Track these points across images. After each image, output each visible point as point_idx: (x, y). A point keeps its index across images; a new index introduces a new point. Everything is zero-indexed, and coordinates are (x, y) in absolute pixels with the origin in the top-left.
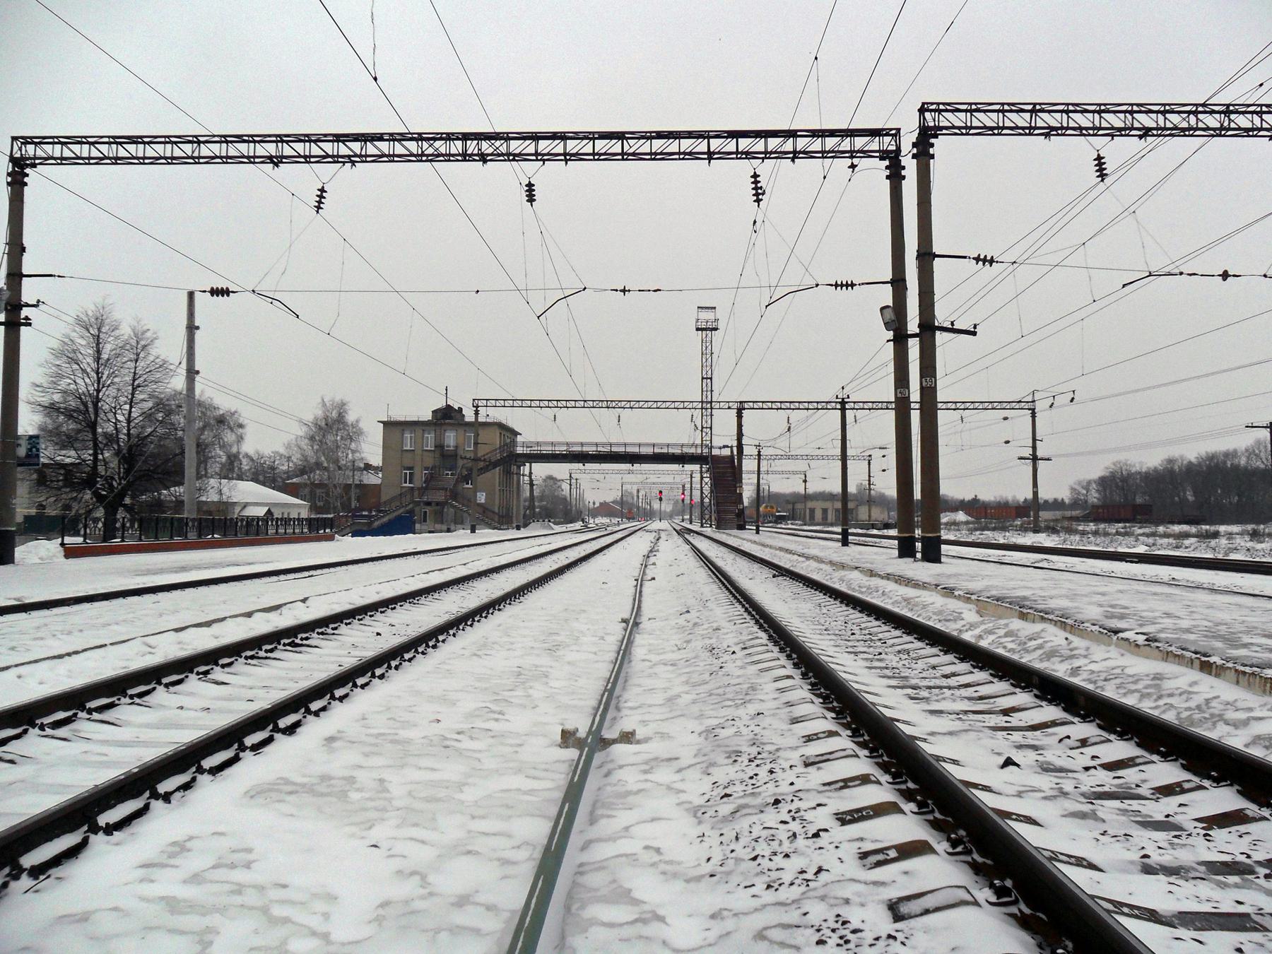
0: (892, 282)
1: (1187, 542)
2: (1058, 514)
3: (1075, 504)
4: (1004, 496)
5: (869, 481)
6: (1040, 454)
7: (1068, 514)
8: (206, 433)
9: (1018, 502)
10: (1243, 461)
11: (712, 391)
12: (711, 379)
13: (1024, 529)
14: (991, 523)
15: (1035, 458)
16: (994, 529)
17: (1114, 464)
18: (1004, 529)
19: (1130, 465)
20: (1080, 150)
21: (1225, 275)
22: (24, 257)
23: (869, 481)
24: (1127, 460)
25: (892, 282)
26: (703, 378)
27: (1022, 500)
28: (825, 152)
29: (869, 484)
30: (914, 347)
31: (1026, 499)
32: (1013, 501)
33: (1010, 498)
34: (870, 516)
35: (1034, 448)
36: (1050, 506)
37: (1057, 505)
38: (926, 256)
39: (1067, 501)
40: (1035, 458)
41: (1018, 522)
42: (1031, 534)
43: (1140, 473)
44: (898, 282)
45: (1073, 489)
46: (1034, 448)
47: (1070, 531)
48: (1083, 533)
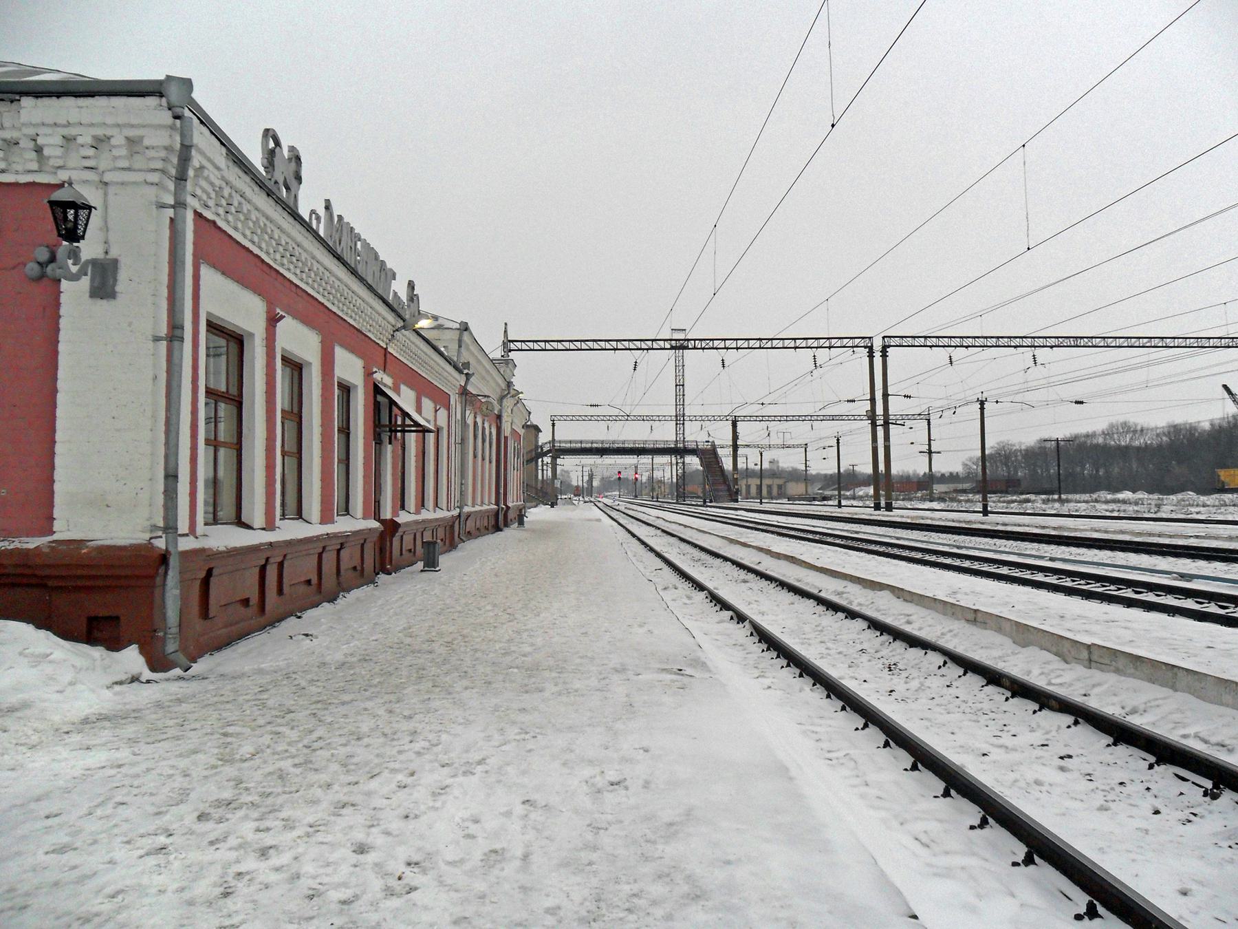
0: (870, 400)
1: (1012, 505)
2: (951, 487)
3: (968, 477)
4: (906, 470)
5: (806, 464)
6: (933, 450)
7: (960, 486)
8: (977, 496)
9: (918, 475)
10: (1101, 440)
11: (684, 395)
12: (683, 385)
13: (923, 499)
14: (899, 495)
15: (930, 452)
16: (903, 500)
17: (998, 444)
18: (910, 500)
19: (1011, 445)
20: (943, 353)
21: (997, 402)
22: (277, 328)
23: (806, 464)
24: (1008, 441)
25: (870, 400)
26: (676, 385)
27: (922, 473)
28: (886, 424)
29: (806, 467)
30: (880, 432)
31: (925, 473)
32: (914, 474)
33: (911, 472)
34: (806, 491)
35: (930, 445)
36: (943, 479)
37: (953, 478)
38: (886, 395)
39: (961, 476)
40: (930, 452)
41: (919, 494)
42: (928, 503)
43: (1021, 451)
44: (873, 400)
45: (965, 465)
46: (930, 445)
47: (952, 500)
48: (960, 501)
